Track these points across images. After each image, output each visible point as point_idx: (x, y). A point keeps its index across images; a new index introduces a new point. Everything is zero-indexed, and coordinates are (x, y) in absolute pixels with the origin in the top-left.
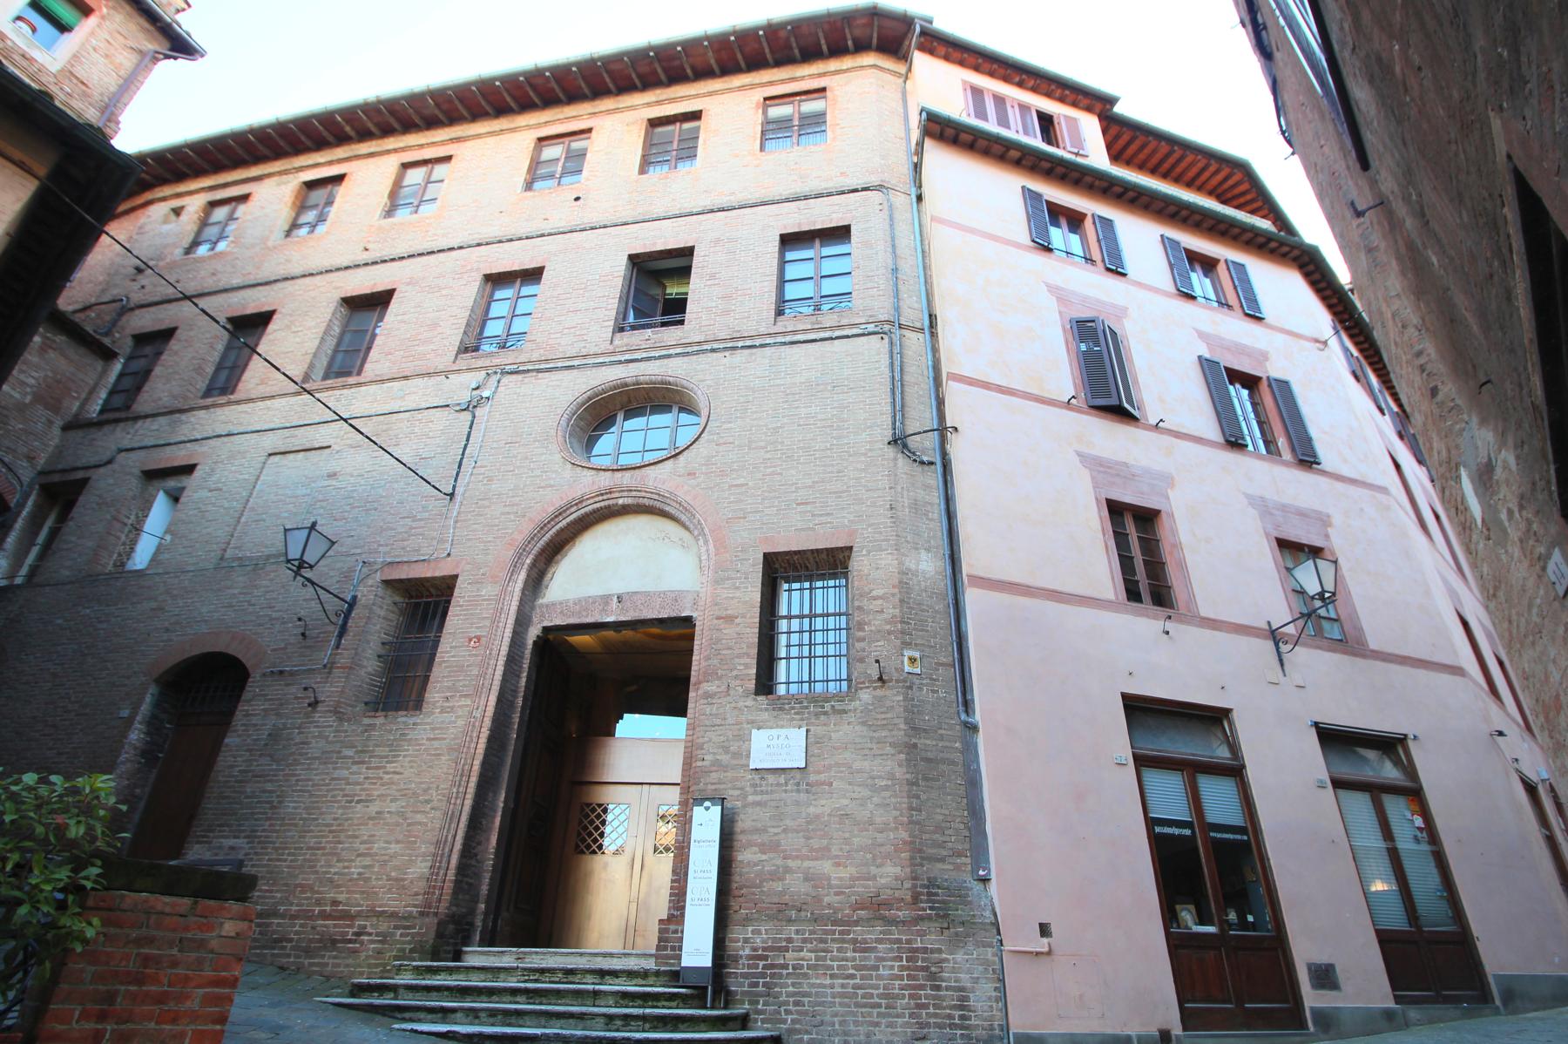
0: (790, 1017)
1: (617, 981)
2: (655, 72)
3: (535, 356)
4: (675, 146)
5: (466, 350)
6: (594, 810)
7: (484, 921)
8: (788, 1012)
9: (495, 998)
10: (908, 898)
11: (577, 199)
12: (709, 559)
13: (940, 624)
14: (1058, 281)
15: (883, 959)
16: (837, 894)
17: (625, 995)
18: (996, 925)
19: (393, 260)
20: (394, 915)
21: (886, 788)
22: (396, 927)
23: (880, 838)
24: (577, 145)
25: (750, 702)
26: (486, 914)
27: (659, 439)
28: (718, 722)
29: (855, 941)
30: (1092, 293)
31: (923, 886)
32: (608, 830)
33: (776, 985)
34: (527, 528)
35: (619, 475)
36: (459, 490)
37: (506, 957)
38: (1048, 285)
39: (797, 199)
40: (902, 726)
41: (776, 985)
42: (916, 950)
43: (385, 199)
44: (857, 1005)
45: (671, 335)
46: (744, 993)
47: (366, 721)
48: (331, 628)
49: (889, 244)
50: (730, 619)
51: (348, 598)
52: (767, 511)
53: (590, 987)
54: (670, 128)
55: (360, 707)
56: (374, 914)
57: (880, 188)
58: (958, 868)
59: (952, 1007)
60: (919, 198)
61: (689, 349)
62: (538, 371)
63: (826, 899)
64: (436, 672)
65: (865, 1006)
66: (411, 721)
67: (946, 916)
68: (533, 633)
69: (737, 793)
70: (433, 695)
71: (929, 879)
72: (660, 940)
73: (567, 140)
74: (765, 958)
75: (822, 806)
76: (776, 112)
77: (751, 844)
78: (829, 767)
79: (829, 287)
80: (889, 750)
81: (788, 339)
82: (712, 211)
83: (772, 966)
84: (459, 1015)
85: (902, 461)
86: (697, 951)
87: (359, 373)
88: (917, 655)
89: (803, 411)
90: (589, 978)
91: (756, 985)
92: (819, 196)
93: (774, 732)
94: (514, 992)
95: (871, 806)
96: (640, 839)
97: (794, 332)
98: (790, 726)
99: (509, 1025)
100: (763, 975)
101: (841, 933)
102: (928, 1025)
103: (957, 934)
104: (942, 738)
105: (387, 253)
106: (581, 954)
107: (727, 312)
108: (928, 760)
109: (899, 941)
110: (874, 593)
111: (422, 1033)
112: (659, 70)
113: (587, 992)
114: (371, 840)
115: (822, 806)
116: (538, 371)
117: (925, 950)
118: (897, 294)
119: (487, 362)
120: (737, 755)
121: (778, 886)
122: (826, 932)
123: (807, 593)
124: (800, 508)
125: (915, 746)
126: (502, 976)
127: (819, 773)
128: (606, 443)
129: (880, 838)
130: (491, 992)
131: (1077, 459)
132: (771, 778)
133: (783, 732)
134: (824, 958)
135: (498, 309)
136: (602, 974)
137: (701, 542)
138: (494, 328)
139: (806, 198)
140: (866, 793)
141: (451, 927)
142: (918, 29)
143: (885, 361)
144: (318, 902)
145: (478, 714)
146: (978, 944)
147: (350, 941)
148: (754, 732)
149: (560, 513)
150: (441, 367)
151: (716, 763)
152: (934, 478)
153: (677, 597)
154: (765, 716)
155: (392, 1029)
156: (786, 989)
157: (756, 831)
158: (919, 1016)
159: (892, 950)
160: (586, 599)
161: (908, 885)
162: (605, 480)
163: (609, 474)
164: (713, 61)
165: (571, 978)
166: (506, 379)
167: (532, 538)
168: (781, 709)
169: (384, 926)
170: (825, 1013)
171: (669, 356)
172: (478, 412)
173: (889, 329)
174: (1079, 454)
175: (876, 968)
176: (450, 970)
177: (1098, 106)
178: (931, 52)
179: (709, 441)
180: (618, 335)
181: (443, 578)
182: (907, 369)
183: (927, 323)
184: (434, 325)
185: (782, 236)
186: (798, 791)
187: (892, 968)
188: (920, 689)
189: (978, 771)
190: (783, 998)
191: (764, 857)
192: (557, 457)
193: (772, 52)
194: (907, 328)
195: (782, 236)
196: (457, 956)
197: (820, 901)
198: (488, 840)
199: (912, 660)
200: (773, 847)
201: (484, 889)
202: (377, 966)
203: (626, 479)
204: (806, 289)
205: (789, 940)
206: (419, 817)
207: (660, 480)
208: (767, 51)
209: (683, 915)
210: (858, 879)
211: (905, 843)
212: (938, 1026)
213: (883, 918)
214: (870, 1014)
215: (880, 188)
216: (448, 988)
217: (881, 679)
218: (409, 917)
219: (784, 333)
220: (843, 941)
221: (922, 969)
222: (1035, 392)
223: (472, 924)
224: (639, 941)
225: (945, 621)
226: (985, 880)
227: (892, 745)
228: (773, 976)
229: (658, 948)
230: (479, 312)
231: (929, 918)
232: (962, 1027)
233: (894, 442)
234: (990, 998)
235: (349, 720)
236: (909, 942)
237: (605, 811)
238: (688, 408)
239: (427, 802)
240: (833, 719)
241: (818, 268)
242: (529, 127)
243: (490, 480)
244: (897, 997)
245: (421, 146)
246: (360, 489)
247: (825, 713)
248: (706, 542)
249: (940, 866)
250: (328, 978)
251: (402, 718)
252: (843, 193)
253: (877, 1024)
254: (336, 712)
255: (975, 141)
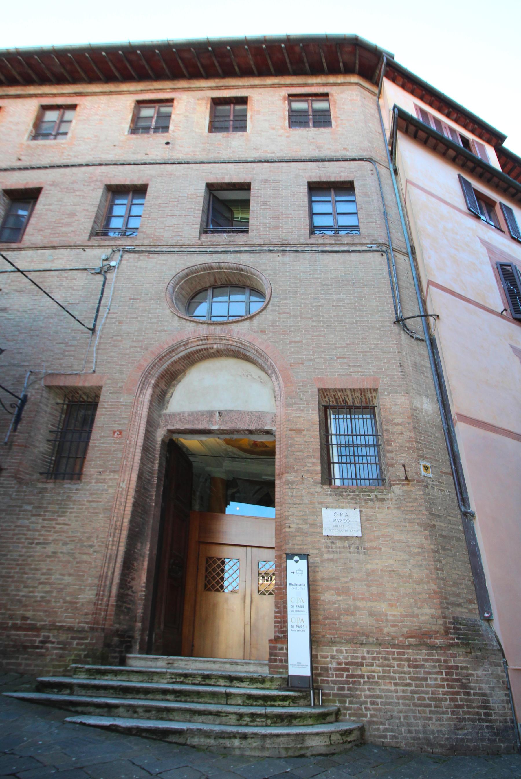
0: (369, 713)
1: (242, 685)
2: (213, 65)
3: (146, 242)
4: (232, 118)
5: (97, 234)
6: (215, 562)
7: (142, 635)
8: (367, 709)
9: (150, 696)
10: (442, 631)
11: (167, 143)
12: (280, 390)
13: (440, 445)
14: (486, 238)
15: (429, 673)
16: (393, 626)
17: (250, 697)
18: (501, 650)
19: (39, 168)
20: (70, 629)
21: (418, 554)
22: (73, 638)
23: (419, 588)
24: (164, 110)
25: (318, 489)
26: (143, 630)
27: (238, 309)
28: (298, 501)
29: (409, 660)
30: (505, 249)
31: (450, 623)
32: (226, 576)
33: (357, 689)
34: (150, 359)
35: (212, 327)
36: (99, 328)
37: (159, 663)
38: (480, 239)
39: (317, 161)
40: (425, 512)
41: (357, 689)
42: (451, 667)
43: (31, 127)
44: (415, 705)
45: (241, 238)
46: (335, 695)
47: (40, 485)
48: (9, 417)
49: (380, 196)
50: (299, 431)
51: (21, 396)
52: (317, 360)
53: (223, 690)
54: (227, 107)
55: (36, 476)
56: (53, 627)
57: (370, 160)
58: (470, 611)
59: (479, 707)
60: (396, 172)
61: (254, 249)
62: (150, 252)
63: (386, 630)
64: (91, 454)
65: (420, 705)
66: (74, 487)
67: (468, 644)
68: (160, 434)
69: (316, 552)
70: (90, 469)
71: (453, 618)
72: (271, 654)
73: (157, 105)
74: (347, 670)
75: (376, 564)
76: (298, 105)
77: (329, 588)
78: (378, 537)
79: (343, 221)
80: (417, 528)
81: (320, 249)
82: (260, 161)
83: (353, 676)
84: (121, 710)
85: (403, 336)
86: (299, 664)
87: (20, 241)
88: (428, 465)
89: (335, 297)
90: (222, 682)
91: (343, 689)
92: (331, 160)
93: (338, 511)
94: (165, 692)
95: (409, 566)
96: (248, 582)
97: (324, 245)
98: (347, 507)
99: (162, 719)
100: (348, 683)
101: (398, 653)
102: (464, 719)
103: (477, 657)
104: (450, 522)
105: (35, 163)
106: (214, 662)
107: (276, 227)
108: (444, 537)
109: (438, 661)
110: (395, 421)
111: (89, 725)
112: (217, 64)
113: (221, 693)
114: (49, 572)
115: (376, 564)
116: (150, 252)
117: (457, 667)
118: (388, 228)
119: (112, 243)
120: (312, 525)
121: (351, 619)
122: (388, 653)
123: (349, 420)
124: (339, 361)
125: (434, 526)
126: (155, 678)
127: (371, 541)
128: (202, 310)
129: (419, 588)
130: (147, 692)
131: (511, 350)
132: (339, 544)
133: (344, 511)
134: (389, 672)
135: (119, 210)
136: (231, 679)
137: (274, 378)
138: (116, 223)
139: (323, 161)
140: (406, 557)
141: (116, 639)
142: (385, 60)
143: (386, 270)
144: (11, 617)
145: (124, 485)
146: (491, 664)
147: (37, 647)
148: (324, 510)
149: (172, 350)
150: (79, 243)
151: (299, 530)
152: (424, 350)
153: (260, 416)
154: (330, 499)
155: (64, 722)
156: (364, 692)
157: (331, 579)
158: (458, 713)
159: (434, 667)
160: (197, 413)
161: (440, 622)
162: (203, 330)
163: (205, 326)
164: (252, 63)
165: (208, 681)
166: (126, 256)
167: (154, 366)
168: (341, 495)
169: (63, 637)
170: (393, 711)
171: (240, 252)
172: (108, 276)
173: (385, 249)
174: (512, 347)
175: (426, 679)
176: (116, 673)
177: (494, 141)
178: (394, 80)
179: (273, 311)
180: (204, 235)
181: (92, 387)
182: (400, 277)
183: (409, 250)
184: (72, 215)
185: (309, 184)
186: (358, 553)
187: (436, 679)
188: (433, 488)
189: (476, 546)
190: (363, 699)
191: (339, 598)
192: (168, 312)
193: (291, 63)
194: (397, 251)
195: (309, 184)
196: (123, 662)
197: (381, 630)
198: (140, 577)
199: (426, 468)
200: (344, 591)
201: (140, 612)
202: (60, 666)
203: (218, 330)
204: (328, 221)
205: (363, 658)
206: (85, 557)
207: (241, 333)
208: (288, 61)
209: (286, 637)
210: (406, 616)
211: (435, 592)
212: (473, 720)
213: (425, 644)
214: (424, 712)
215: (370, 160)
216: (112, 688)
217: (406, 478)
218: (82, 631)
219: (317, 245)
220: (401, 660)
221: (457, 680)
222: (481, 303)
223: (132, 637)
224: (254, 651)
225: (442, 445)
226: (489, 620)
227: (419, 524)
228: (354, 683)
229: (270, 660)
230: (105, 210)
231: (457, 645)
232: (487, 721)
233: (397, 321)
234: (503, 701)
235: (27, 484)
236: (445, 661)
237: (223, 563)
238: (256, 291)
239: (91, 546)
240: (377, 504)
241: (334, 208)
242: (129, 92)
243: (121, 322)
244: (441, 700)
245: (54, 95)
246: (26, 321)
247: (371, 500)
248: (277, 378)
249: (459, 609)
250: (22, 675)
251: (68, 485)
252: (346, 160)
253: (430, 719)
254: (16, 478)
255: (427, 139)
